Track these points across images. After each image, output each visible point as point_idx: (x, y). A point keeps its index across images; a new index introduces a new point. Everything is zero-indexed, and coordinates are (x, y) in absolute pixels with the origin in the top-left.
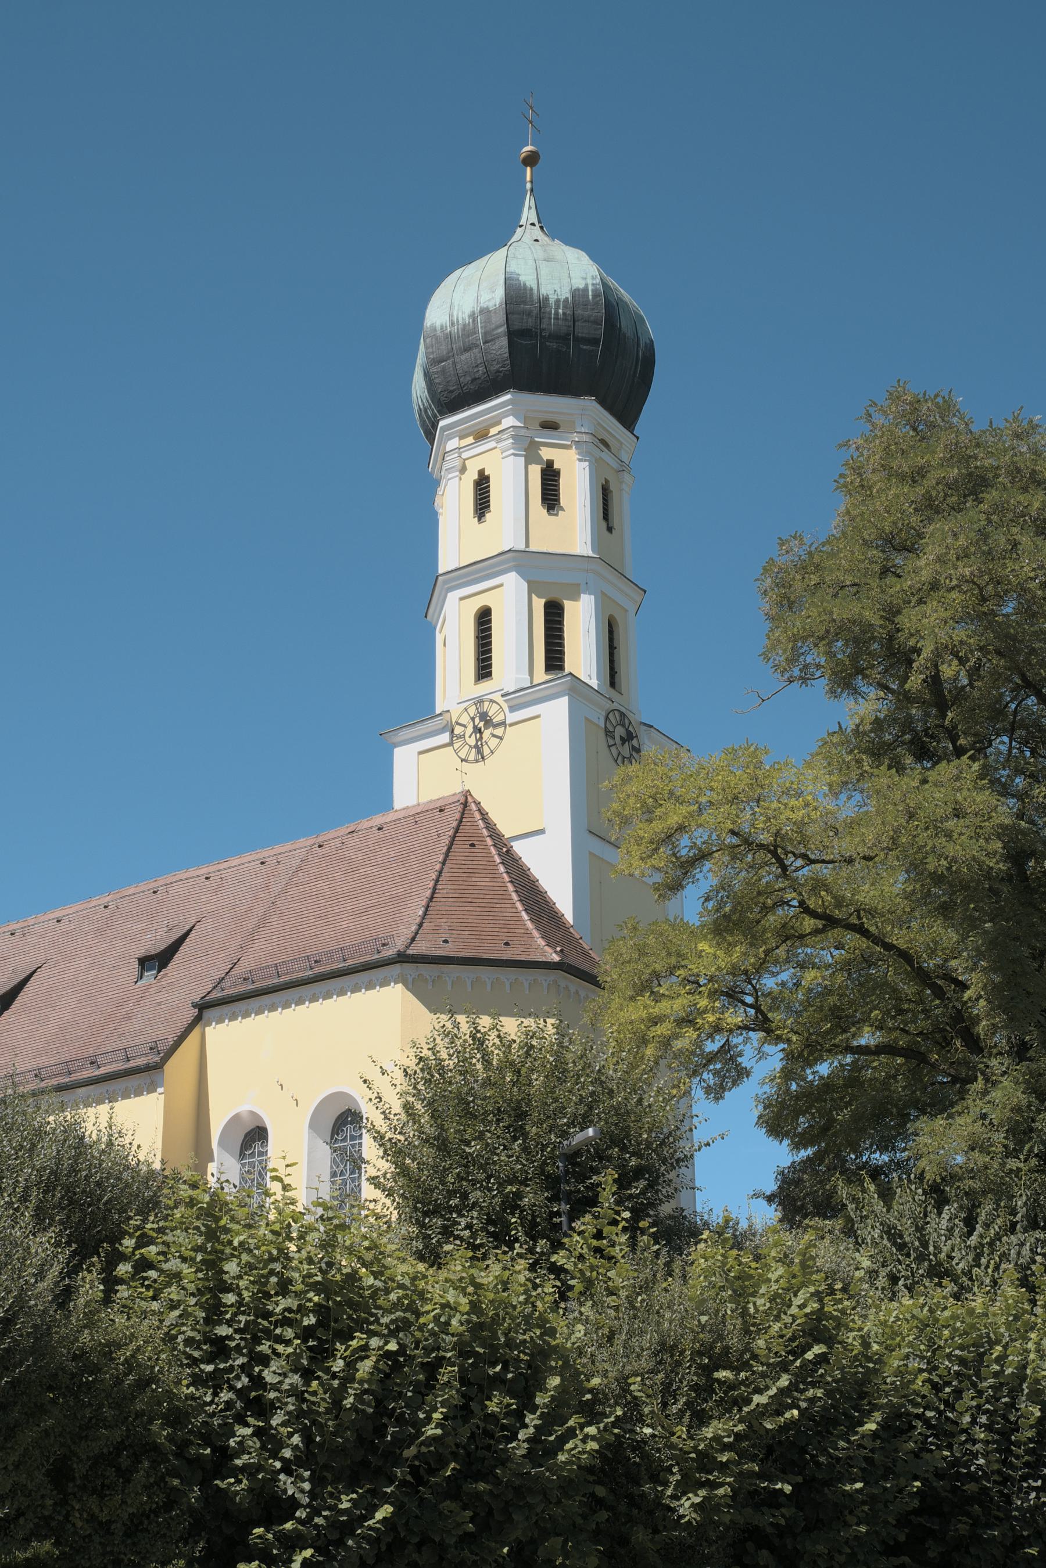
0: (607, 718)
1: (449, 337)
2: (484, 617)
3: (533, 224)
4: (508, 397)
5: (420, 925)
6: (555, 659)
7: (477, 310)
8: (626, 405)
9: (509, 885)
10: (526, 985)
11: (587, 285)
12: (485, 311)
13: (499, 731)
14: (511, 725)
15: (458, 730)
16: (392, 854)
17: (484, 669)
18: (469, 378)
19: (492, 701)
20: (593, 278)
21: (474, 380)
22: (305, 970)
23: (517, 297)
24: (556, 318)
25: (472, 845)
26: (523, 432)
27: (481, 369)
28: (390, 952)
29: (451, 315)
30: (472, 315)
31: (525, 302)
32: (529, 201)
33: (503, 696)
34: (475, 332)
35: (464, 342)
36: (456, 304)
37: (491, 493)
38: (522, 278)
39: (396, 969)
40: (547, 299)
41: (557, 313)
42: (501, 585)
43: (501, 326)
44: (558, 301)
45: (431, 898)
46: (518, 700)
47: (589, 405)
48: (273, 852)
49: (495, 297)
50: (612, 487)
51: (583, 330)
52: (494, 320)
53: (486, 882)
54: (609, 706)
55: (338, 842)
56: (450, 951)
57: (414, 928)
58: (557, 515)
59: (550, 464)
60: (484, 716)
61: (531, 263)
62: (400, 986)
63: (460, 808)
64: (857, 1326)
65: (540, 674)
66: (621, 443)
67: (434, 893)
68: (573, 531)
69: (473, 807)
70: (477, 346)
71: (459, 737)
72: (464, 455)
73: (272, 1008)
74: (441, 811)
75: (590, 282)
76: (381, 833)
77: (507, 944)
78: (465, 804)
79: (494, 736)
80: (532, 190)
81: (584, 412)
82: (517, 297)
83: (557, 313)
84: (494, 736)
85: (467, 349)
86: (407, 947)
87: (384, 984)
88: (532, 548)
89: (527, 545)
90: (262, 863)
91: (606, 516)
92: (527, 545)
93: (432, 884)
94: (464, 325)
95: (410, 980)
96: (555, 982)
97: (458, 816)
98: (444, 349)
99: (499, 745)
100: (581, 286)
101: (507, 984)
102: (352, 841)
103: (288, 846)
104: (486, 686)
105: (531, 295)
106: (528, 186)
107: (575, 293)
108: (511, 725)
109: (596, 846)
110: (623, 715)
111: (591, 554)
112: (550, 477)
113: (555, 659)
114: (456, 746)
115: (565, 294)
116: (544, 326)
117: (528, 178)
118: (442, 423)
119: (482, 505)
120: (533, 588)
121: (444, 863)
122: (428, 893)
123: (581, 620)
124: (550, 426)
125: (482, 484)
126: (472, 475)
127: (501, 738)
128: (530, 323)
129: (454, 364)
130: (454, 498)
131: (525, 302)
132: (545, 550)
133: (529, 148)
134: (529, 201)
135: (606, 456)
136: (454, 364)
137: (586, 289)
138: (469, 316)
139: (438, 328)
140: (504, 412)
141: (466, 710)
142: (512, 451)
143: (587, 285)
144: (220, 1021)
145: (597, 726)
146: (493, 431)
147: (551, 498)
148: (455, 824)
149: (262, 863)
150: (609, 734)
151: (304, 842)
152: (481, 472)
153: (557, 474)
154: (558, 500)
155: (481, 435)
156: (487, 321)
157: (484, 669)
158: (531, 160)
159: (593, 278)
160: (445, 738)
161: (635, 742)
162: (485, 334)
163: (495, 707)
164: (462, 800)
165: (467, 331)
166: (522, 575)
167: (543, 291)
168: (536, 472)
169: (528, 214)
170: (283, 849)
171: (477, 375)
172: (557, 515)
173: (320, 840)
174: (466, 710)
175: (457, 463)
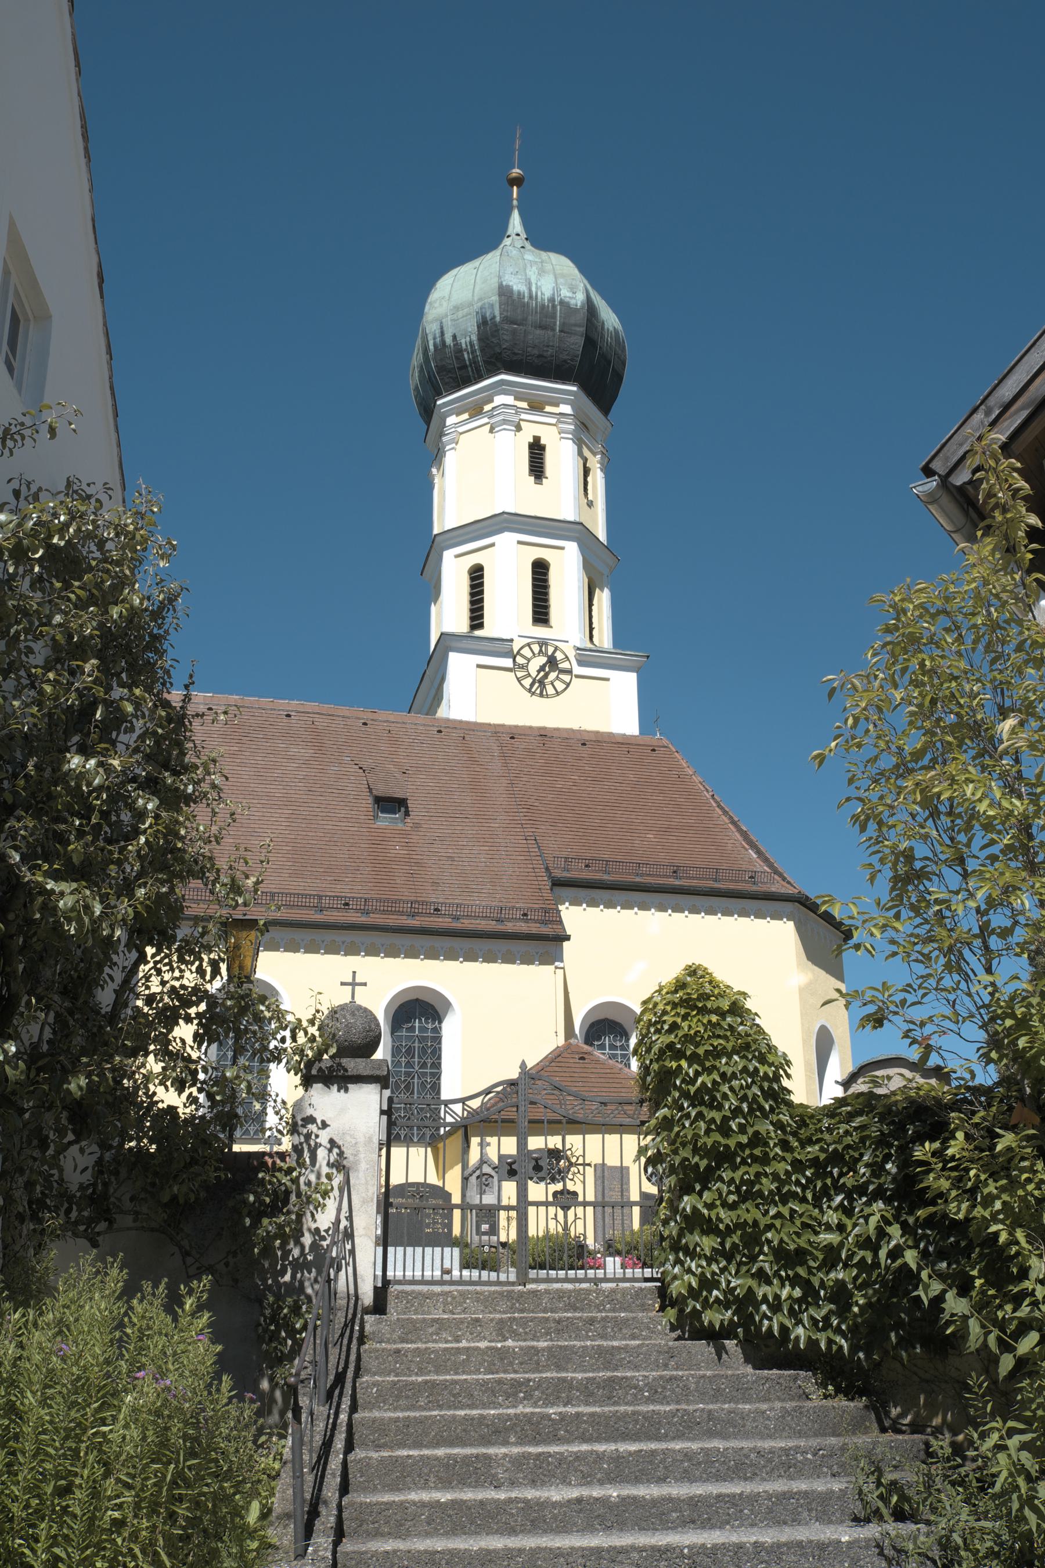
1: (525, 306)
2: (540, 569)
4: (575, 389)
13: (566, 678)
14: (577, 676)
18: (536, 352)
21: (540, 356)
30: (552, 300)
34: (554, 316)
38: (515, 288)
39: (789, 907)
64: (285, 1166)
72: (523, 416)
73: (694, 910)
85: (543, 327)
108: (577, 676)
125: (537, 451)
152: (537, 439)
153: (543, 448)
158: (518, 181)
160: (508, 663)
162: (563, 325)
169: (516, 223)
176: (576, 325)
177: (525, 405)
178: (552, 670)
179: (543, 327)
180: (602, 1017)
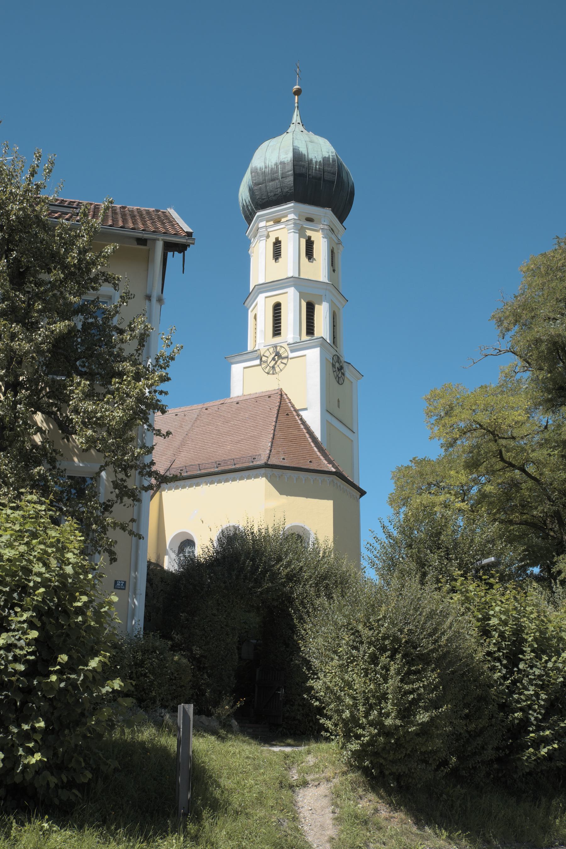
0: (333, 358)
2: (277, 307)
3: (299, 123)
4: (292, 204)
5: (271, 451)
6: (310, 330)
7: (278, 162)
8: (342, 213)
9: (306, 434)
10: (320, 481)
11: (329, 156)
12: (282, 163)
13: (285, 361)
14: (291, 359)
15: (264, 359)
16: (247, 416)
17: (277, 331)
18: (272, 194)
19: (281, 347)
20: (332, 153)
21: (275, 195)
22: (214, 467)
23: (299, 159)
24: (316, 170)
25: (287, 414)
26: (298, 222)
27: (279, 190)
28: (262, 462)
29: (265, 163)
30: (276, 164)
31: (301, 161)
32: (296, 112)
33: (288, 345)
34: (277, 172)
35: (271, 177)
36: (268, 158)
37: (282, 249)
38: (301, 149)
39: (263, 471)
40: (311, 160)
41: (316, 168)
42: (286, 293)
43: (290, 171)
44: (316, 162)
45: (273, 438)
46: (295, 347)
47: (328, 212)
48: (181, 410)
49: (288, 157)
50: (335, 251)
51: (327, 177)
52: (287, 168)
53: (296, 432)
54: (335, 353)
55: (216, 408)
56: (286, 463)
57: (268, 452)
58: (312, 262)
59: (310, 238)
60: (278, 354)
61: (304, 142)
62: (264, 479)
63: (279, 396)
65: (305, 337)
66: (339, 231)
67: (274, 436)
68: (318, 270)
69: (285, 396)
70: (278, 179)
71: (265, 362)
72: (269, 230)
74: (269, 397)
75: (331, 154)
76: (238, 405)
77: (310, 462)
78: (281, 395)
79: (282, 363)
80: (298, 107)
81: (325, 214)
82: (299, 159)
83: (316, 168)
84: (282, 363)
85: (273, 180)
86: (268, 461)
87: (256, 477)
88: (302, 277)
89: (299, 275)
90: (176, 415)
91: (332, 265)
92: (299, 275)
93: (272, 432)
94: (272, 169)
95: (269, 476)
96: (333, 480)
97: (279, 400)
98: (261, 179)
99: (284, 368)
100: (327, 156)
101: (312, 481)
102: (223, 408)
103: (188, 408)
104: (277, 340)
105: (305, 158)
106: (296, 105)
107: (324, 159)
108: (291, 359)
109: (329, 417)
110: (338, 357)
111: (327, 281)
112: (310, 244)
113: (310, 330)
114: (263, 366)
115: (320, 159)
116: (310, 173)
117: (296, 101)
118: (258, 214)
119: (277, 254)
120: (302, 296)
121: (276, 422)
122: (272, 436)
123: (322, 313)
124: (310, 220)
125: (277, 244)
126: (272, 240)
127: (286, 364)
128: (304, 171)
129: (266, 186)
130: (260, 251)
131: (301, 161)
132: (307, 278)
133: (297, 87)
134: (296, 112)
135: (333, 237)
136: (266, 186)
137: (329, 158)
138: (275, 165)
139: (259, 168)
140: (290, 211)
141: (268, 350)
142: (292, 230)
143: (329, 156)
144: (170, 489)
145: (330, 362)
146: (283, 220)
147: (310, 254)
148: (278, 404)
149: (176, 415)
150: (333, 366)
151: (200, 406)
152: (277, 239)
153: (280, 242)
154: (312, 255)
155: (277, 221)
156: (283, 168)
157: (277, 331)
158: (298, 92)
159: (332, 153)
160: (257, 362)
161: (342, 371)
162: (282, 174)
163: (283, 350)
164: (280, 393)
165: (274, 172)
166: (296, 288)
167: (310, 157)
168: (303, 242)
169: (296, 118)
170: (187, 409)
171: (277, 193)
172: (312, 262)
173: (206, 406)
174: (268, 350)
175: (266, 233)
176: (288, 171)
177: (272, 223)
178: (278, 359)
179: (273, 180)
180: (185, 539)
